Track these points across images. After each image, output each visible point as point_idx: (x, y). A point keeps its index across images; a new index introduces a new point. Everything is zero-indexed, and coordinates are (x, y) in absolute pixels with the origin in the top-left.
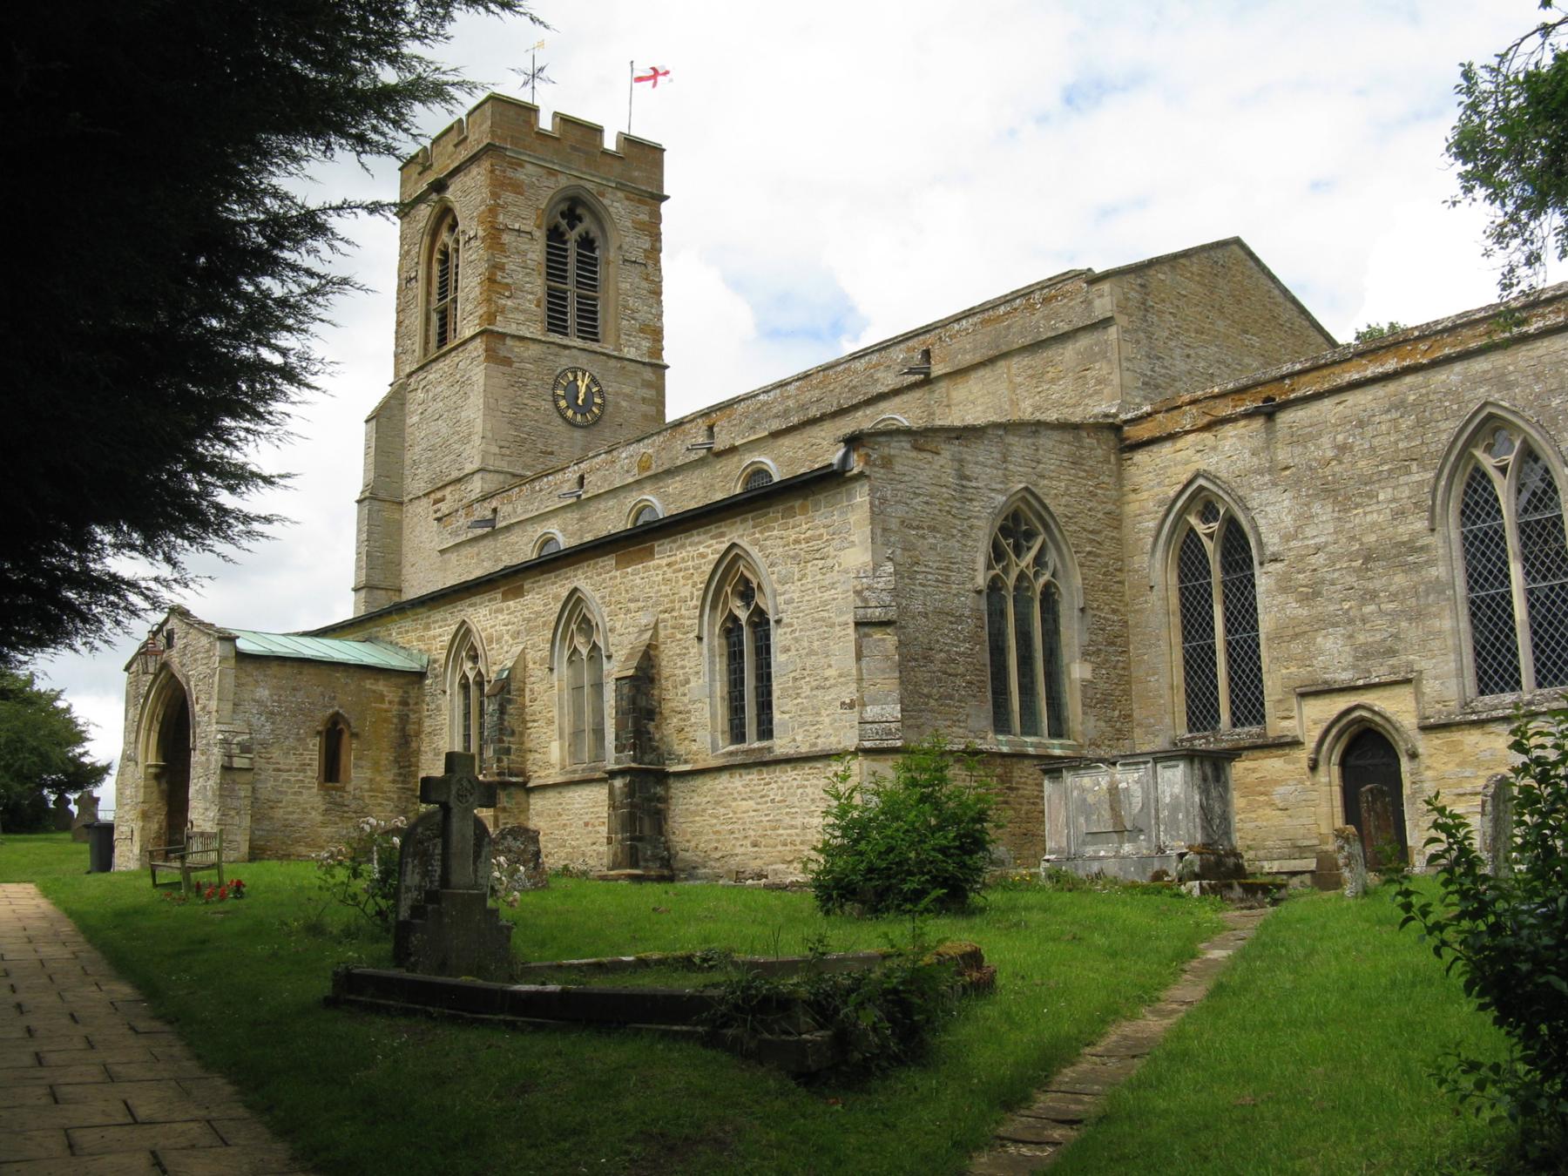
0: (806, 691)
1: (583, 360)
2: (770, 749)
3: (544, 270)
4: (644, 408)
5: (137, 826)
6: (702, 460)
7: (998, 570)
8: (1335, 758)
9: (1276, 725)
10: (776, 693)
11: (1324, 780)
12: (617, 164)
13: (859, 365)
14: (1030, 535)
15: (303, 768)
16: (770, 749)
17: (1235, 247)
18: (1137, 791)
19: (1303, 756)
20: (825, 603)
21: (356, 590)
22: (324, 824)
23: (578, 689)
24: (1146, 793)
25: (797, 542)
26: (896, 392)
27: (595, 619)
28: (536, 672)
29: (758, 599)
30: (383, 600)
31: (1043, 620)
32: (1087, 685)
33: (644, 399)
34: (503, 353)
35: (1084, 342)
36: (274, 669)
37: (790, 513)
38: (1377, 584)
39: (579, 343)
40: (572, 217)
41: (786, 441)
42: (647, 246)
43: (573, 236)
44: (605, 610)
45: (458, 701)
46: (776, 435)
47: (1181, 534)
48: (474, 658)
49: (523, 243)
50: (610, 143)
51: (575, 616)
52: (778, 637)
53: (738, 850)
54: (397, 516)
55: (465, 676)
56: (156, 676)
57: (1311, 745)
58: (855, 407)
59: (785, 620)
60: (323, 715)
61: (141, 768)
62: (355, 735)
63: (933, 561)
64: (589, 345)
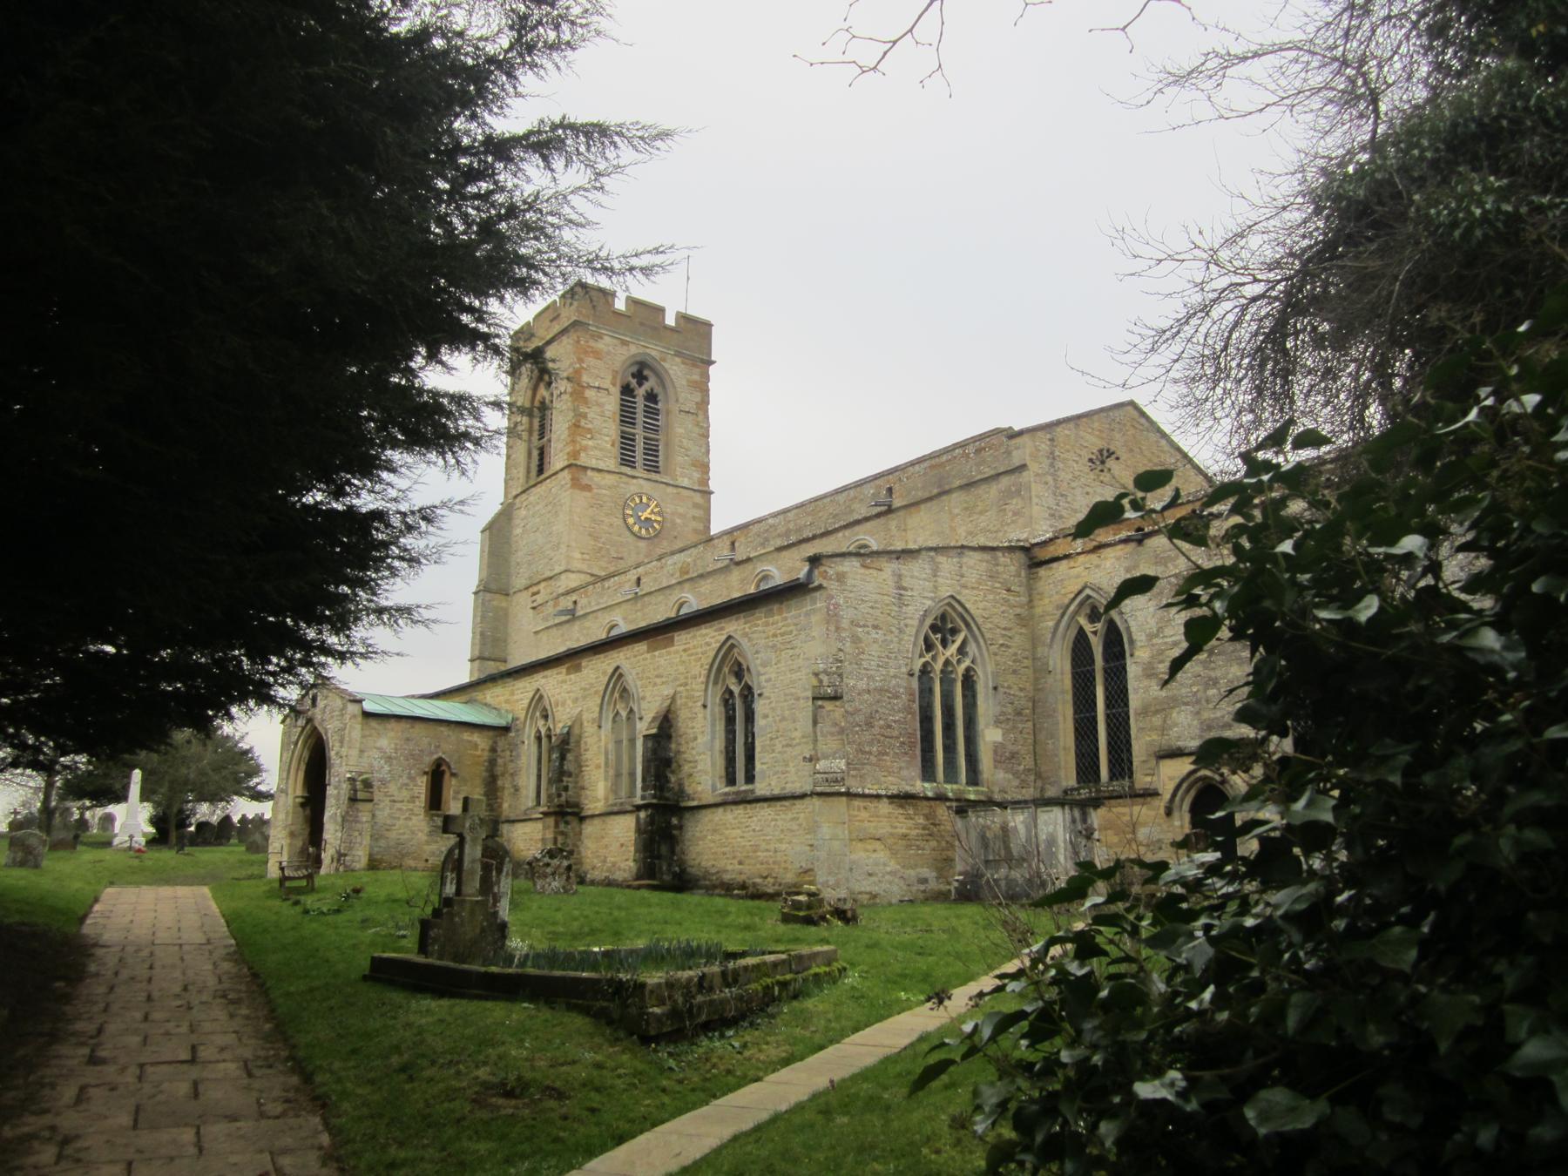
0: (779, 747)
1: (647, 486)
2: (752, 791)
3: (618, 418)
4: (695, 524)
5: (286, 842)
6: (727, 567)
7: (928, 657)
8: (1186, 806)
9: (1142, 780)
10: (758, 749)
11: (1177, 823)
12: (676, 335)
13: (841, 498)
14: (954, 631)
15: (413, 799)
16: (752, 791)
17: (1130, 408)
18: (1022, 829)
19: (1160, 804)
20: (793, 682)
21: (472, 660)
22: (428, 843)
23: (618, 742)
24: (1028, 830)
25: (775, 635)
26: (867, 519)
27: (632, 688)
28: (590, 729)
29: (746, 678)
30: (493, 668)
31: (964, 696)
32: (997, 749)
33: (694, 518)
34: (585, 481)
35: (1005, 481)
36: (393, 724)
37: (770, 614)
38: (1218, 673)
39: (646, 474)
40: (640, 377)
41: (785, 554)
42: (698, 399)
43: (640, 392)
44: (639, 683)
45: (534, 749)
46: (780, 549)
47: (1073, 633)
48: (546, 717)
49: (602, 397)
50: (670, 320)
51: (618, 686)
52: (760, 707)
53: (729, 868)
54: (504, 604)
55: (539, 731)
56: (303, 728)
57: (1167, 796)
58: (814, 537)
59: (766, 694)
60: (428, 761)
61: (290, 798)
62: (453, 775)
63: (875, 650)
64: (654, 476)
